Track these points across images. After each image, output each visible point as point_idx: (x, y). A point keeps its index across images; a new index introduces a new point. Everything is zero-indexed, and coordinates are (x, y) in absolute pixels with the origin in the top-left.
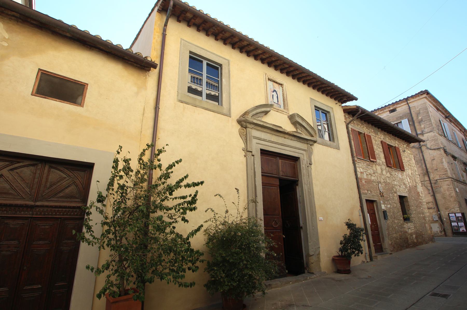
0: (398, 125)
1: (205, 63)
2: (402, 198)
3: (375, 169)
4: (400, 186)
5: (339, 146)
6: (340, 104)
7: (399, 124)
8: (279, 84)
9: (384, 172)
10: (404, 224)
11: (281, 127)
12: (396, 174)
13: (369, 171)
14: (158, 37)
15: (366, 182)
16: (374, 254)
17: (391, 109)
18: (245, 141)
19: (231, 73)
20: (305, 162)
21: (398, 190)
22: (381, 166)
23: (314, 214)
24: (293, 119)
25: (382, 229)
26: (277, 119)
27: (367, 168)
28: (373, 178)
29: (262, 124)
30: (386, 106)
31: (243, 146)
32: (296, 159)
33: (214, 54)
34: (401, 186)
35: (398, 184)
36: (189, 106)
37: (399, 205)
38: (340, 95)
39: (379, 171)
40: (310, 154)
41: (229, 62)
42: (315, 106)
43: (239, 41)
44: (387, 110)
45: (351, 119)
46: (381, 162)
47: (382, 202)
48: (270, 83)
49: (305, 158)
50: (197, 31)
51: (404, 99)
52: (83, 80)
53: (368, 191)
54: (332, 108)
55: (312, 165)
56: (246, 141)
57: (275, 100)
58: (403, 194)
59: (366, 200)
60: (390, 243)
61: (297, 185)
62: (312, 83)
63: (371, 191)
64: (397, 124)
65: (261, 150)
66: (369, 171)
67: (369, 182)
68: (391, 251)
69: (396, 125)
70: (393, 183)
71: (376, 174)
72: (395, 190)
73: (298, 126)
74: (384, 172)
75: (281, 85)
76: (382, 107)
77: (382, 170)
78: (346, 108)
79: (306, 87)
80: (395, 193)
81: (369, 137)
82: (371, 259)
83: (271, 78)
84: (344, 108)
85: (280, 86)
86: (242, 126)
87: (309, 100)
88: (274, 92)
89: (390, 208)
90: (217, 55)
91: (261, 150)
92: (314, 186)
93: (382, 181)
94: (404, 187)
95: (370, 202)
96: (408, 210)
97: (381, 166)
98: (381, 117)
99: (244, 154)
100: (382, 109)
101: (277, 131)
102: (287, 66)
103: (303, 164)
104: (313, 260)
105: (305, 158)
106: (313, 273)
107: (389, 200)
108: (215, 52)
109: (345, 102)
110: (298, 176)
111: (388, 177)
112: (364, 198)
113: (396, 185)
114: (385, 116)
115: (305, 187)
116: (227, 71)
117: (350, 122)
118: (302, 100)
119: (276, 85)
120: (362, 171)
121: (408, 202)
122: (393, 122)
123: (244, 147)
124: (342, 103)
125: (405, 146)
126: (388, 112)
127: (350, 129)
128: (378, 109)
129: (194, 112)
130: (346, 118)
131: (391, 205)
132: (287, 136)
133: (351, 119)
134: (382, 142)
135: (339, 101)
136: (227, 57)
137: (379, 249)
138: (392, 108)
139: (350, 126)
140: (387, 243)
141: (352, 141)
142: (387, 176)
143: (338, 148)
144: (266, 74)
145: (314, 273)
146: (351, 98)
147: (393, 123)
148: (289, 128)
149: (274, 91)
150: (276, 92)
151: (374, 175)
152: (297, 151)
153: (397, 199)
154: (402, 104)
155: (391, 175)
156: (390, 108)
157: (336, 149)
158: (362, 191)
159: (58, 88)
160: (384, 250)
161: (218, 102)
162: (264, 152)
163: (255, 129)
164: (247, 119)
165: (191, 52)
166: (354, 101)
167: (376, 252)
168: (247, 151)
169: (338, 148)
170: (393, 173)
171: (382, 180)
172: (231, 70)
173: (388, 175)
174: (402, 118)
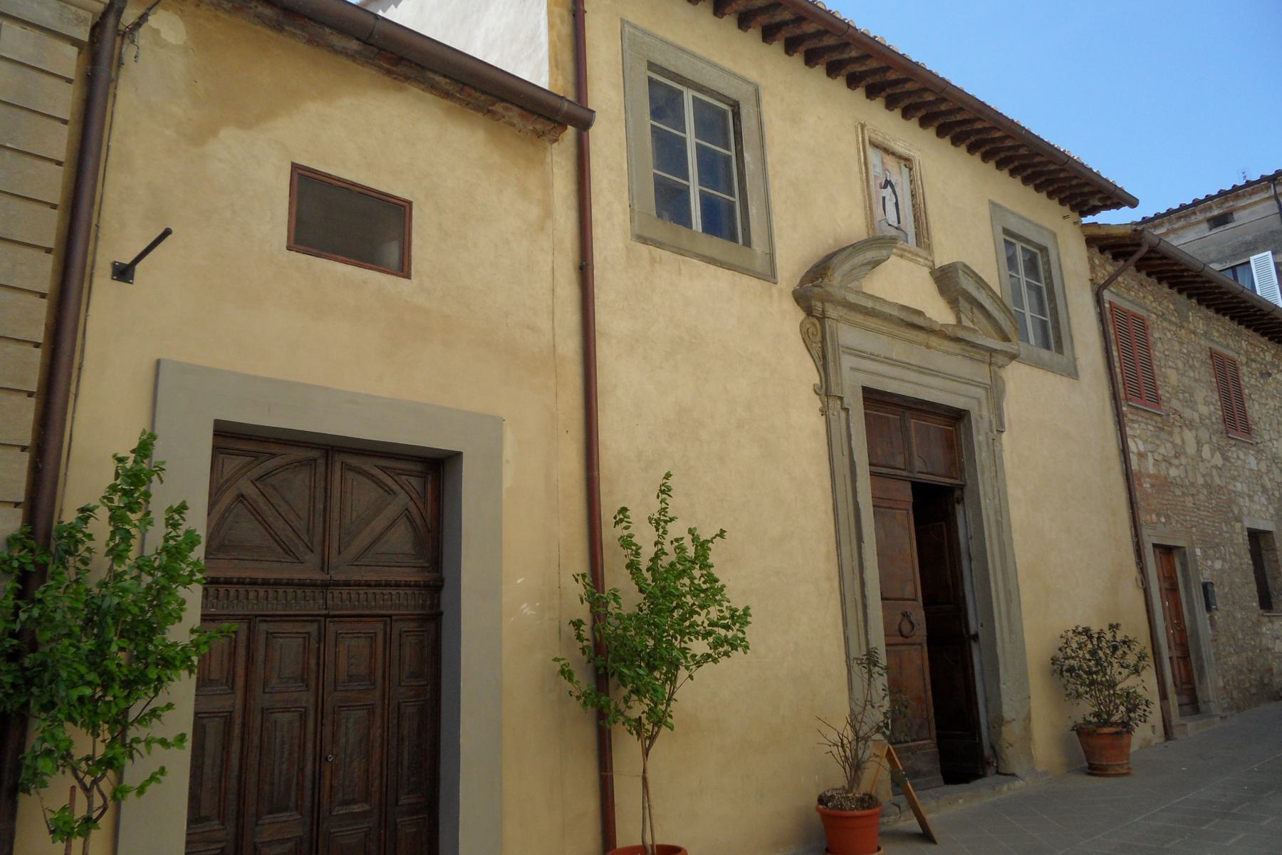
0: (1236, 278)
1: (688, 96)
2: (1257, 539)
3: (1178, 441)
4: (1250, 497)
5: (1075, 366)
6: (1075, 216)
7: (1239, 270)
8: (900, 157)
9: (1206, 451)
10: (1258, 624)
11: (920, 313)
12: (1242, 456)
13: (1162, 450)
14: (562, 22)
15: (1152, 486)
16: (1175, 718)
17: (1216, 212)
18: (820, 363)
19: (766, 129)
20: (984, 426)
21: (1245, 511)
22: (1197, 429)
23: (1012, 596)
24: (947, 280)
25: (1198, 637)
26: (903, 283)
27: (1158, 437)
28: (1173, 472)
29: (869, 304)
30: (1196, 203)
31: (815, 379)
32: (957, 417)
33: (715, 65)
34: (1256, 498)
35: (1246, 490)
36: (665, 254)
37: (1247, 560)
38: (1077, 188)
39: (1191, 449)
40: (995, 392)
41: (757, 91)
42: (1006, 231)
43: (793, 22)
44: (1200, 217)
45: (1110, 269)
46: (1196, 416)
47: (1198, 552)
48: (874, 157)
49: (985, 413)
50: (740, 27)
51: (1263, 178)
52: (399, 191)
53: (1158, 515)
54: (906, 161)
55: (1004, 435)
56: (824, 362)
57: (892, 218)
58: (1262, 525)
59: (1155, 546)
60: (1221, 684)
61: (960, 500)
62: (967, 135)
63: (1167, 517)
64: (1233, 268)
65: (865, 389)
66: (1162, 450)
67: (1163, 484)
68: (1224, 710)
69: (1229, 274)
70: (1231, 487)
71: (1183, 460)
72: (1236, 511)
73: (963, 304)
74: (1206, 451)
75: (907, 159)
76: (1183, 207)
77: (1199, 444)
78: (1096, 231)
79: (838, 86)
80: (1238, 519)
81: (1143, 325)
82: (1168, 734)
83: (879, 138)
84: (1090, 231)
85: (903, 163)
86: (809, 312)
87: (985, 211)
88: (885, 187)
89: (1222, 571)
90: (723, 70)
91: (865, 389)
92: (1011, 505)
93: (1200, 481)
94: (1263, 500)
95: (1166, 551)
96: (1275, 579)
97: (1197, 429)
98: (1175, 243)
99: (820, 405)
100: (1183, 212)
101: (911, 323)
102: (931, 98)
103: (978, 432)
104: (1011, 733)
105: (985, 413)
106: (1013, 775)
107: (1218, 545)
108: (716, 59)
109: (1094, 210)
110: (962, 470)
111: (1216, 467)
112: (1149, 539)
113: (1241, 494)
114: (1189, 242)
115: (987, 506)
116: (754, 122)
117: (1112, 279)
118: (966, 206)
119: (891, 162)
120: (1142, 449)
121: (1274, 549)
122: (1219, 261)
123: (817, 381)
124: (1083, 214)
125: (1268, 357)
126: (1205, 226)
127: (1107, 305)
128: (1170, 212)
129: (680, 274)
130: (1093, 269)
131: (1224, 560)
132: (934, 341)
133: (1110, 269)
134: (1213, 355)
135: (1073, 209)
136: (752, 74)
137: (1193, 704)
138: (1218, 209)
139: (1107, 295)
140: (1213, 685)
141: (1114, 348)
142: (1214, 462)
143: (1072, 372)
144: (863, 127)
145: (1018, 771)
146: (1116, 198)
147: (1216, 267)
148: (938, 312)
149: (888, 183)
150: (892, 186)
151: (1176, 462)
152: (963, 388)
153: (1242, 540)
154: (1256, 198)
155: (1226, 459)
156: (1210, 208)
157: (1069, 375)
158: (1144, 517)
159: (349, 223)
160: (1203, 707)
161: (733, 238)
162: (873, 398)
163: (848, 321)
164: (830, 289)
165: (652, 66)
166: (1125, 209)
167: (1182, 715)
168: (826, 391)
169: (1072, 372)
170: (1233, 453)
171: (1199, 477)
172: (765, 117)
173: (1217, 459)
174: (1254, 247)
